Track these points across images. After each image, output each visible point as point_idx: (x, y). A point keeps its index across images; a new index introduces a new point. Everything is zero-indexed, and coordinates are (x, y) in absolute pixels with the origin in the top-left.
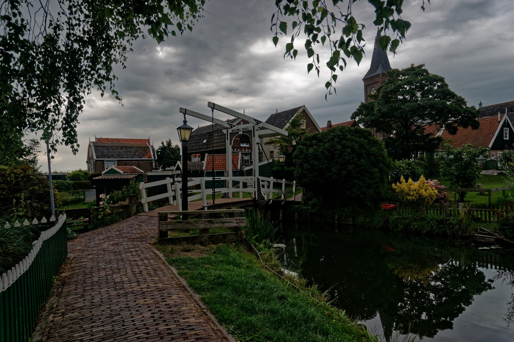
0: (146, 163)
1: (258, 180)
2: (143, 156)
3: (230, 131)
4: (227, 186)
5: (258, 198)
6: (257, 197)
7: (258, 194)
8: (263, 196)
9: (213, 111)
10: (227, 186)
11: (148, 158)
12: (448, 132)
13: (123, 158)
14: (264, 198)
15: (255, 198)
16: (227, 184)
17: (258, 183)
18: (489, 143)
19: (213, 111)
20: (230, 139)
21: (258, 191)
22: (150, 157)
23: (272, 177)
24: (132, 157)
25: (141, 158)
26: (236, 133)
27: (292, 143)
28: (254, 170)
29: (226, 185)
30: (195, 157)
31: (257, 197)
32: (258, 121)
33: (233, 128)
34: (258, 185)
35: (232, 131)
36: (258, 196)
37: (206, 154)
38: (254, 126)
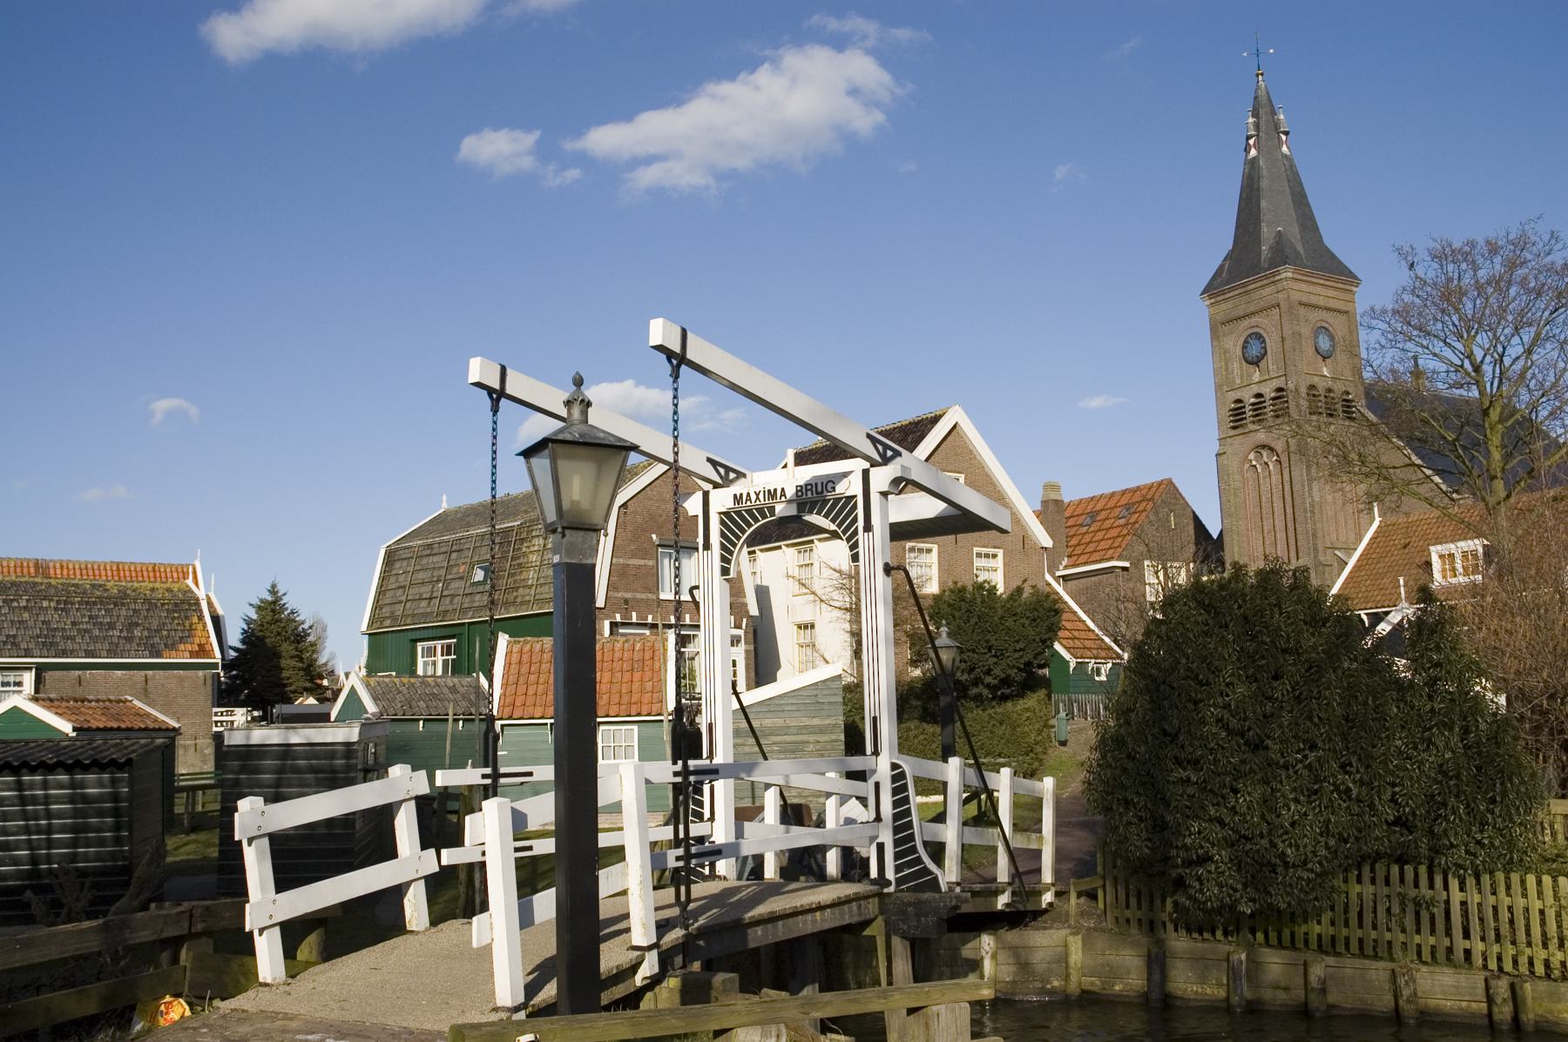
0: (181, 679)
1: (895, 779)
2: (172, 646)
3: (722, 500)
4: (707, 815)
5: (899, 881)
6: (890, 874)
7: (897, 856)
8: (926, 871)
9: (495, 410)
10: (707, 815)
11: (193, 654)
12: (248, 621)
13: (64, 654)
14: (936, 879)
15: (882, 881)
16: (706, 799)
17: (895, 792)
18: (509, 654)
19: (495, 410)
20: (723, 547)
21: (897, 843)
22: (203, 650)
23: (397, 771)
24: (112, 653)
25: (159, 655)
26: (761, 511)
27: (1147, 559)
28: (875, 719)
29: (700, 804)
30: (431, 652)
31: (890, 874)
32: (728, 469)
33: (738, 488)
34: (896, 804)
35: (737, 499)
36: (898, 869)
37: (503, 640)
38: (866, 473)
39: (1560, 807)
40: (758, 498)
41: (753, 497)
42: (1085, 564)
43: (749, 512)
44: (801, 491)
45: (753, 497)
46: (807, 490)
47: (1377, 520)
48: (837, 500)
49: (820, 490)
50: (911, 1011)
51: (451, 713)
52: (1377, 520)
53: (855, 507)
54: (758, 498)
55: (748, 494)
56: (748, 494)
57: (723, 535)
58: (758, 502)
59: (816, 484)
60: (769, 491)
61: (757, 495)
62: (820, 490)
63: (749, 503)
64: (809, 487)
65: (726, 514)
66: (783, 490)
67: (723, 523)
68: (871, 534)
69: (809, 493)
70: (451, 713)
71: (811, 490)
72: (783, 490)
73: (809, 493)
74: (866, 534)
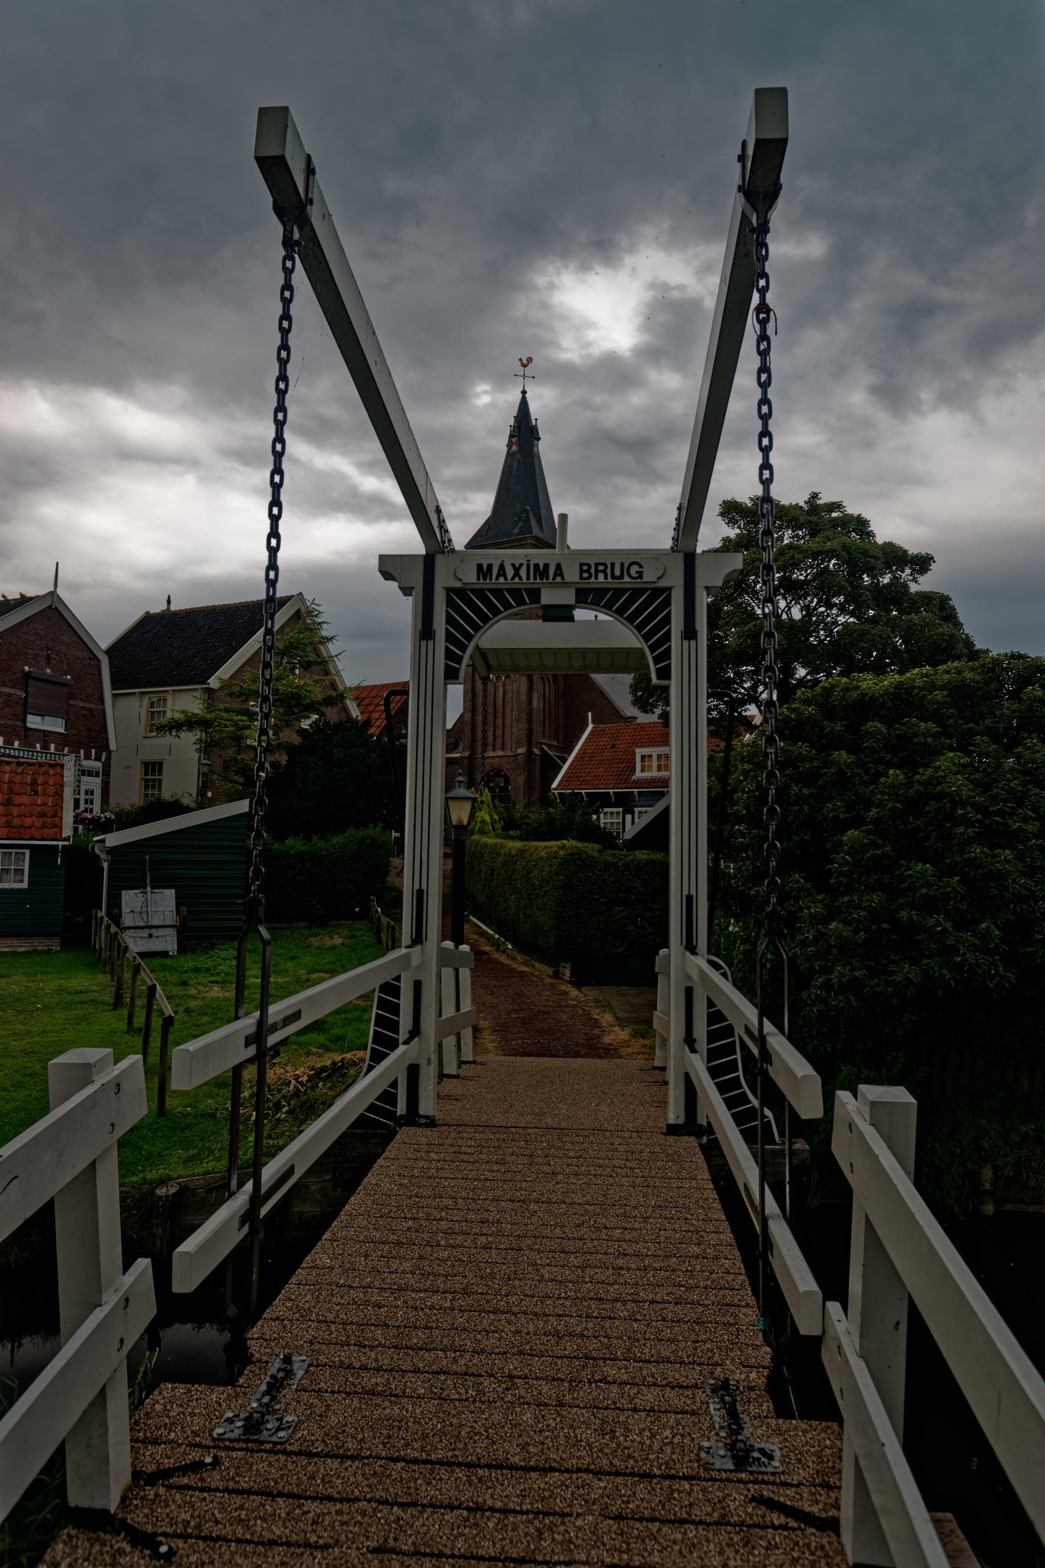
20: (449, 638)
39: (428, 1565)
40: (517, 574)
41: (510, 572)
42: (625, 788)
43: (498, 593)
44: (588, 571)
45: (510, 572)
46: (597, 571)
47: (591, 726)
48: (637, 593)
49: (617, 573)
50: (126, 768)
51: (149, 893)
52: (591, 726)
53: (667, 602)
54: (517, 574)
55: (502, 567)
56: (502, 567)
57: (450, 620)
58: (517, 580)
59: (613, 565)
60: (536, 566)
61: (517, 570)
62: (617, 573)
63: (517, 580)
64: (601, 568)
65: (461, 592)
66: (559, 567)
67: (450, 603)
68: (431, 643)
69: (601, 576)
70: (149, 893)
71: (604, 572)
72: (559, 567)
73: (601, 576)
74: (424, 643)
